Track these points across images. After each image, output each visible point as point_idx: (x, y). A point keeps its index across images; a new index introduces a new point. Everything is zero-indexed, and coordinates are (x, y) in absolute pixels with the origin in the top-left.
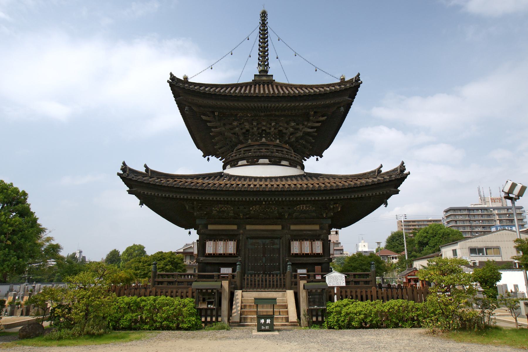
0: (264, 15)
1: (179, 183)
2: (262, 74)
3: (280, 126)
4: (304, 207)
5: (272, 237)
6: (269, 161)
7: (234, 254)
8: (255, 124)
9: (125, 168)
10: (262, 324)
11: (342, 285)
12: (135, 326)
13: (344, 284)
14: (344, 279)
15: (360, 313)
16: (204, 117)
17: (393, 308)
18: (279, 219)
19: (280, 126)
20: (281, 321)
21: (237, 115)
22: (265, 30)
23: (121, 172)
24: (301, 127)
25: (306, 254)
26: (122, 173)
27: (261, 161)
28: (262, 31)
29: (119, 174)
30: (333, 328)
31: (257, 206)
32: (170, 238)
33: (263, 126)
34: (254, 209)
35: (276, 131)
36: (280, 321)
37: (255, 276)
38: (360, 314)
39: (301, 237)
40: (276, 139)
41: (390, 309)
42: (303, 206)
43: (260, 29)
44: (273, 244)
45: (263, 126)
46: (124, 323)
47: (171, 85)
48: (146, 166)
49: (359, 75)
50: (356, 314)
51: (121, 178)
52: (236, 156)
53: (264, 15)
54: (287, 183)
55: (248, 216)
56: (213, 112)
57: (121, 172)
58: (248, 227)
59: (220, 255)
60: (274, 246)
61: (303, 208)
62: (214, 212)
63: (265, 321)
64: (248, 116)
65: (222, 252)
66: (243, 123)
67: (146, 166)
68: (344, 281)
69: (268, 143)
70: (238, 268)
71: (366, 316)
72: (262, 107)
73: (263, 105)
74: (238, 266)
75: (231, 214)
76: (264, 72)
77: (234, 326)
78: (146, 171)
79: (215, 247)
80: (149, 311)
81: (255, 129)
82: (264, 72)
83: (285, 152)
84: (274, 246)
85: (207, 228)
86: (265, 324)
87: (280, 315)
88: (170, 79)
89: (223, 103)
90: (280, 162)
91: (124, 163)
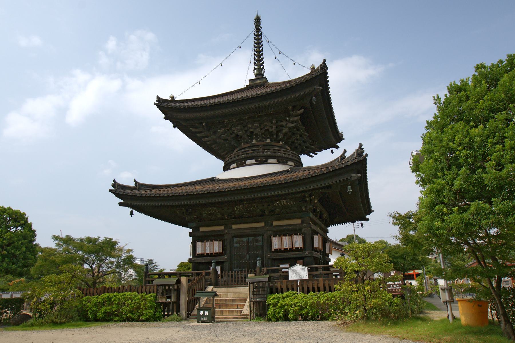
0: (258, 20)
2: (258, 77)
3: (266, 126)
4: (284, 202)
5: (255, 234)
6: (256, 161)
8: (274, 121)
9: (115, 184)
10: (201, 316)
11: (304, 278)
12: (108, 318)
13: (307, 277)
14: (307, 272)
15: (295, 305)
16: (193, 129)
17: (331, 300)
18: (261, 216)
19: (266, 126)
20: (236, 314)
21: (224, 122)
22: (260, 35)
24: (284, 123)
25: (285, 249)
26: (113, 189)
27: (248, 162)
29: (110, 191)
30: (271, 321)
31: (241, 206)
33: (250, 128)
34: (238, 209)
35: (263, 131)
36: (235, 314)
38: (295, 306)
39: (280, 232)
40: (266, 139)
41: (326, 300)
42: (283, 202)
43: (254, 34)
44: (257, 241)
45: (250, 128)
46: (100, 315)
48: (135, 181)
50: (291, 306)
51: (113, 193)
52: (235, 157)
53: (258, 20)
55: (233, 216)
56: (201, 123)
58: (234, 227)
59: (286, 250)
60: (258, 244)
61: (284, 204)
62: (204, 215)
63: (204, 313)
64: (234, 122)
65: (288, 247)
66: (231, 129)
67: (135, 181)
68: (307, 274)
69: (259, 143)
70: (258, 264)
71: (302, 308)
72: (256, 108)
73: (257, 105)
74: (258, 262)
75: (219, 216)
77: (193, 319)
78: (135, 184)
79: (203, 248)
80: (118, 304)
81: (274, 127)
83: (272, 151)
84: (258, 244)
86: (204, 316)
87: (238, 308)
88: (157, 101)
89: (209, 113)
90: (267, 161)
91: (114, 181)
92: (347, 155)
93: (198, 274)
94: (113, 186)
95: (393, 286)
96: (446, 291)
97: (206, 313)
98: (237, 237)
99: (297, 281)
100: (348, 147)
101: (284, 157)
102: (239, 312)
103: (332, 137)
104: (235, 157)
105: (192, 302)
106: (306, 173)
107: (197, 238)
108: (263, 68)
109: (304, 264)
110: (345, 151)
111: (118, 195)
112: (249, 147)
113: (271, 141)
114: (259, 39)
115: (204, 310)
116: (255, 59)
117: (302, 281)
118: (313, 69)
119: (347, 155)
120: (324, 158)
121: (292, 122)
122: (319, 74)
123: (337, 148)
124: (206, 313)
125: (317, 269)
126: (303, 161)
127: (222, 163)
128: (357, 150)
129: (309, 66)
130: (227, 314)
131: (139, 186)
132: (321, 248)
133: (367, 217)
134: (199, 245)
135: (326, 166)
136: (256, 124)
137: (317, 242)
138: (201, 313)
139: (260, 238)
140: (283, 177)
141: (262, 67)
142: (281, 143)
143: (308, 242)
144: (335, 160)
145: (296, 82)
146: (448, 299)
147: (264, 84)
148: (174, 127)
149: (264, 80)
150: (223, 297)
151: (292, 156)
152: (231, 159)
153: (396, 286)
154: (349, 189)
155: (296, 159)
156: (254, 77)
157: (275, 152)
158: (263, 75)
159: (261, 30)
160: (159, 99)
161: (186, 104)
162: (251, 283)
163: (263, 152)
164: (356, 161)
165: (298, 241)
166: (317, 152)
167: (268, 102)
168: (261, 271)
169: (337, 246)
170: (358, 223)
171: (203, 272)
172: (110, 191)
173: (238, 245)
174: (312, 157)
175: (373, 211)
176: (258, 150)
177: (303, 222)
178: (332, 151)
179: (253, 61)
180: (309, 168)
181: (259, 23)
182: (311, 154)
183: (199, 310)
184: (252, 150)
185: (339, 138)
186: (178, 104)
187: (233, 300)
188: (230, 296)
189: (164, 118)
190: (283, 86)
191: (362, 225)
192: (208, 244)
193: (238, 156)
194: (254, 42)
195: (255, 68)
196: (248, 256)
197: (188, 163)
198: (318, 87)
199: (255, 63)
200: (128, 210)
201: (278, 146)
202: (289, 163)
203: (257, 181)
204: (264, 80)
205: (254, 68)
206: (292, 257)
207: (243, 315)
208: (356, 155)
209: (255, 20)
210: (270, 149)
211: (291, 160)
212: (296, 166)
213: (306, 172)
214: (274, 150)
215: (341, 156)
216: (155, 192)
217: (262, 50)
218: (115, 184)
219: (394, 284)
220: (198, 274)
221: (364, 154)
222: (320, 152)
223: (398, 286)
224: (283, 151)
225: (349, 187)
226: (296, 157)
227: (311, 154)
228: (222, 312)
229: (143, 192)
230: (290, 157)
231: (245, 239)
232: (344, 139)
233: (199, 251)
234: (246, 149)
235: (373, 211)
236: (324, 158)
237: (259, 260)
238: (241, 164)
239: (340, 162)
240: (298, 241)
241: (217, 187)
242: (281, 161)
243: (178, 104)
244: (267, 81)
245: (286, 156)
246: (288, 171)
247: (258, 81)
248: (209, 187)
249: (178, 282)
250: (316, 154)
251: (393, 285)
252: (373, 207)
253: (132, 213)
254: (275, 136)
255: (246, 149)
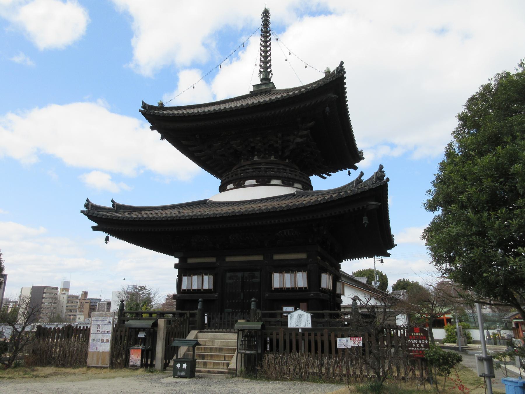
1: (144, 215)
5: (250, 268)
6: (256, 182)
7: (305, 288)
14: (310, 319)
22: (267, 32)
23: (85, 209)
27: (248, 182)
28: (263, 32)
29: (82, 212)
32: (157, 274)
36: (221, 367)
37: (233, 314)
40: (270, 156)
47: (144, 114)
48: (112, 201)
49: (342, 63)
51: (86, 215)
54: (276, 204)
57: (85, 209)
58: (228, 259)
60: (254, 280)
63: (182, 366)
67: (112, 201)
68: (310, 322)
74: (253, 303)
76: (266, 79)
78: (113, 205)
82: (266, 79)
83: (276, 170)
84: (254, 280)
85: (186, 261)
86: (181, 369)
87: (225, 360)
88: (142, 107)
90: (270, 182)
91: (87, 200)
92: (364, 178)
93: (181, 315)
94: (86, 206)
95: (416, 347)
96: (485, 363)
97: (185, 366)
98: (230, 271)
99: (297, 329)
100: (366, 168)
101: (291, 178)
102: (225, 365)
103: (350, 156)
104: (232, 176)
105: (170, 351)
106: (314, 199)
107: (183, 270)
108: (271, 71)
109: (308, 310)
110: (362, 174)
111: (91, 217)
112: (249, 165)
113: (275, 158)
114: (267, 37)
115: (182, 362)
116: (261, 60)
117: (304, 329)
118: (328, 72)
119: (364, 178)
120: (338, 180)
121: (301, 137)
122: (334, 79)
123: (355, 168)
124: (185, 366)
125: (323, 316)
126: (313, 184)
127: (218, 182)
128: (377, 173)
129: (324, 70)
130: (212, 366)
131: (117, 207)
132: (330, 287)
133: (389, 251)
134: (185, 279)
135: (338, 191)
136: (258, 138)
137: (326, 281)
138: (179, 365)
139: (257, 274)
140: (284, 204)
141: (269, 70)
142: (287, 161)
143: (314, 281)
144: (349, 184)
145: (306, 89)
146: (486, 373)
147: (270, 91)
148: (162, 139)
149: (271, 86)
150: (209, 345)
151: (300, 177)
152: (228, 178)
153: (420, 347)
154: (365, 220)
155: (304, 180)
156: (259, 82)
157: (280, 172)
158: (270, 80)
159: (270, 26)
160: (144, 105)
161: (176, 112)
162: (241, 330)
163: (266, 171)
164: (374, 186)
165: (301, 280)
166: (331, 173)
167: (273, 112)
168: (255, 314)
169: (352, 281)
170: (377, 259)
171: (187, 312)
172: (82, 212)
173: (230, 281)
174: (325, 178)
175: (396, 245)
176: (260, 168)
177: (308, 257)
178: (349, 173)
179: (258, 62)
180: (318, 193)
181: (268, 17)
182: (324, 175)
183: (176, 362)
184: (253, 169)
185: (358, 156)
186: (165, 112)
187: (220, 350)
188: (217, 344)
189: (151, 128)
190: (290, 94)
191: (382, 261)
192: (195, 278)
193: (236, 175)
194: (261, 40)
195: (260, 72)
196: (242, 296)
197: (179, 180)
198: (333, 96)
199: (261, 66)
200: (104, 235)
201: (284, 165)
202: (296, 185)
203: (248, 206)
204: (271, 86)
205: (260, 71)
206: (295, 298)
207: (230, 369)
208: (374, 179)
209: (263, 13)
210: (273, 168)
211: (299, 182)
212: (304, 189)
213: (314, 197)
214: (278, 169)
215: (357, 180)
216: (135, 215)
217: (270, 49)
218: (88, 204)
219: (418, 343)
220: (181, 315)
221: (385, 178)
222: (334, 172)
223: (422, 346)
224: (290, 171)
225: (365, 218)
226: (304, 178)
227: (324, 175)
228: (205, 364)
229: (120, 215)
230: (297, 178)
231: (240, 275)
232: (363, 158)
233: (184, 287)
234: (246, 167)
235: (396, 245)
236: (338, 180)
237: (254, 301)
238: (239, 185)
239: (355, 187)
240: (301, 280)
241: (207, 212)
242: (286, 183)
243: (165, 112)
244: (274, 87)
245: (293, 176)
246: (293, 195)
247: (264, 87)
248: (198, 212)
249: (155, 325)
250: (330, 175)
251: (416, 344)
252: (397, 240)
253: (107, 239)
254: (280, 153)
255: (246, 167)
